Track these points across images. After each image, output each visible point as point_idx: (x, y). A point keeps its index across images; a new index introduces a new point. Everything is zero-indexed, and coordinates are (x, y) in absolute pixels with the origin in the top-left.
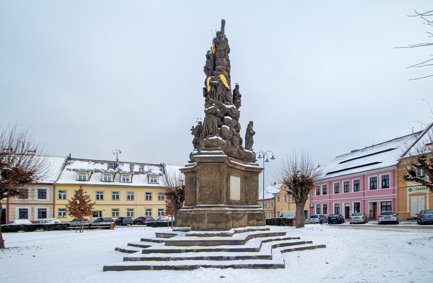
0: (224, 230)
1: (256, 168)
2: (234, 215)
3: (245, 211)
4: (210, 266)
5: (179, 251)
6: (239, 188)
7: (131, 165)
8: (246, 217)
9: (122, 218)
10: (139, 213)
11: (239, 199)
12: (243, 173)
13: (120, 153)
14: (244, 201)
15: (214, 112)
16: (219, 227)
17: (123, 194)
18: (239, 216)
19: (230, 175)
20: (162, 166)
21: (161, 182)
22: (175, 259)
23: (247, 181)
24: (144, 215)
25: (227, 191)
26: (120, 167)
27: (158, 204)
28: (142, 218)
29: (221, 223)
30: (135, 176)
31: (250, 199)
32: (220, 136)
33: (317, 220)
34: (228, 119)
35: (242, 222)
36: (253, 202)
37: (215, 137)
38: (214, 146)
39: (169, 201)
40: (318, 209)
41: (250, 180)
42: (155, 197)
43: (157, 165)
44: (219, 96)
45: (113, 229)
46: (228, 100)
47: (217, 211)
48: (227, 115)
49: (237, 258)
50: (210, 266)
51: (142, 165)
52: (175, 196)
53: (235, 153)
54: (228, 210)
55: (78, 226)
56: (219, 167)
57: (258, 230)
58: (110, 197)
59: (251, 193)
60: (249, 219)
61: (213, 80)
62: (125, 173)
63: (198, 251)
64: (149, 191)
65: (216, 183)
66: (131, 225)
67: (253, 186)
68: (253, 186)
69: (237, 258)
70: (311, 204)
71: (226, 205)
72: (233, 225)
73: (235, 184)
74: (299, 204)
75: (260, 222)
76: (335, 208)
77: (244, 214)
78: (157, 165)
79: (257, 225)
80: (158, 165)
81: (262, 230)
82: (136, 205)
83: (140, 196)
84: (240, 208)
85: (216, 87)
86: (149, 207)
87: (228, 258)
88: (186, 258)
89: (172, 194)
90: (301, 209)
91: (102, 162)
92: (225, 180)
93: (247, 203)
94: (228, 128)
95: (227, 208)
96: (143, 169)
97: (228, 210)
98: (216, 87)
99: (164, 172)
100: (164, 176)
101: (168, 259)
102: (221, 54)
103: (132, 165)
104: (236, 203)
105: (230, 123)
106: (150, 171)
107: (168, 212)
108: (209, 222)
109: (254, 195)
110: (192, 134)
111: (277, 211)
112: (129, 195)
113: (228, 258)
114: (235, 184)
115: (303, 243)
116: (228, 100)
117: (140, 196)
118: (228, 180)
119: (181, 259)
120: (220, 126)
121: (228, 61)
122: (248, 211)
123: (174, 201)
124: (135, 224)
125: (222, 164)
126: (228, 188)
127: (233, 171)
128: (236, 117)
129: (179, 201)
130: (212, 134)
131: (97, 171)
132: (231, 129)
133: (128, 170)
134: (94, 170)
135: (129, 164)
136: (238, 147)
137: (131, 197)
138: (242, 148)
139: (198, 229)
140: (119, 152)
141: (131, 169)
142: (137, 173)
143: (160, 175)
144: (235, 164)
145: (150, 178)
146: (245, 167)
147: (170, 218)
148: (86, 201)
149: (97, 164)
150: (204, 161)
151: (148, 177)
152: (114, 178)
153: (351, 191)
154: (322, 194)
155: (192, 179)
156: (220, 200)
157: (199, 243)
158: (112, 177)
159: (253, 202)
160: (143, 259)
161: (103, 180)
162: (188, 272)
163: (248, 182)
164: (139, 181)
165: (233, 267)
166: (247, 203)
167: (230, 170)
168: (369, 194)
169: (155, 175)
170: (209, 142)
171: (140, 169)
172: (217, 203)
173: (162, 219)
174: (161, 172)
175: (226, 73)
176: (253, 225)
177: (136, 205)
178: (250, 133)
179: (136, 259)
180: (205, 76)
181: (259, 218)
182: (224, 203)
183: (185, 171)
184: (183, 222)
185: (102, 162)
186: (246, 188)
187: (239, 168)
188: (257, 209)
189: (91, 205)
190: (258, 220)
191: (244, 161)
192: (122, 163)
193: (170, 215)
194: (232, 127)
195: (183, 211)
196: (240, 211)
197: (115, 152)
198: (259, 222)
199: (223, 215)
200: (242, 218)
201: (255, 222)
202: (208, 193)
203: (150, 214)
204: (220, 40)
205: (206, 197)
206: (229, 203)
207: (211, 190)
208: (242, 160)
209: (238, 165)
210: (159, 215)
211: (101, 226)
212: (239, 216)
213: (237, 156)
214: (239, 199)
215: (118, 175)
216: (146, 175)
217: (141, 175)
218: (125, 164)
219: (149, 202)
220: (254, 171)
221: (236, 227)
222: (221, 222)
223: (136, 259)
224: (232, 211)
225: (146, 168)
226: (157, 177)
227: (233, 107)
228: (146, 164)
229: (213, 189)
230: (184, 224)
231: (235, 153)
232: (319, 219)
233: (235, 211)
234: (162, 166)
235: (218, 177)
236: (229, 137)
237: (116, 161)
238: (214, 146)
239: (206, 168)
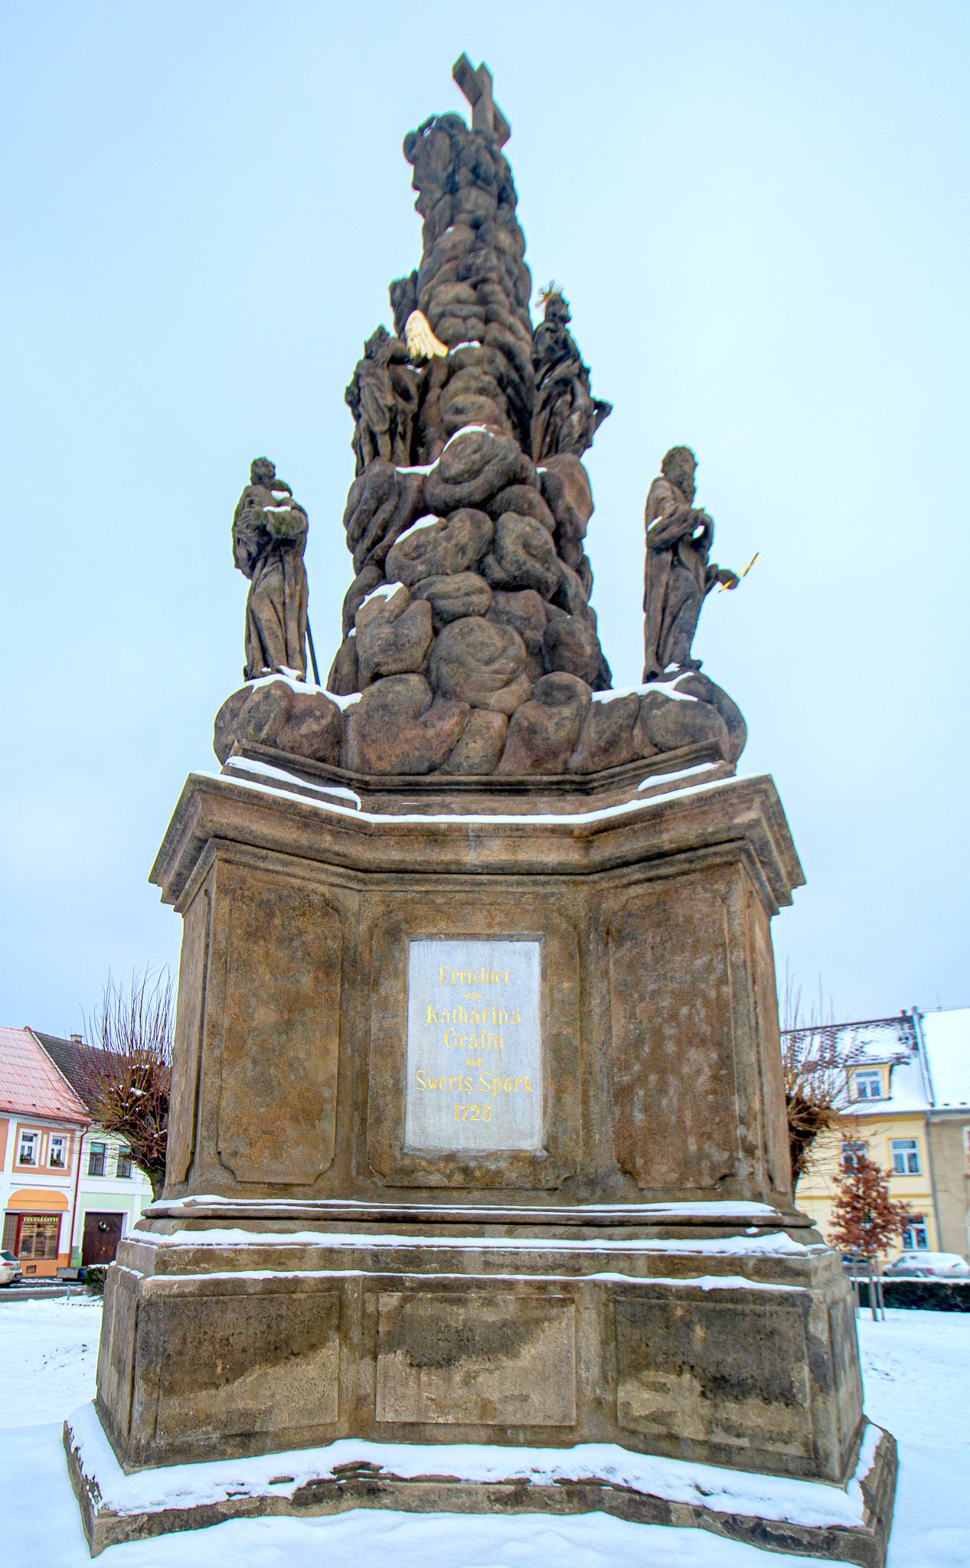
2: (390, 1301)
3: (573, 1263)
8: (575, 1337)
11: (532, 1142)
12: (575, 898)
14: (605, 1158)
18: (459, 1316)
23: (626, 951)
31: (657, 1129)
35: (494, 1382)
36: (687, 1165)
41: (651, 937)
43: (889, 1022)
51: (832, 1031)
59: (662, 1066)
60: (627, 1359)
75: (752, 1414)
77: (552, 1298)
78: (889, 1022)
79: (718, 1455)
80: (894, 1020)
96: (833, 1047)
100: (914, 1062)
104: (470, 1175)
109: (703, 1082)
121: (516, 232)
122: (607, 1261)
143: (899, 1060)
159: (687, 1165)
171: (822, 1049)
173: (910, 1264)
174: (903, 1049)
176: (660, 1441)
178: (681, 549)
181: (736, 1361)
186: (617, 1029)
187: (495, 853)
188: (710, 1247)
190: (718, 1385)
196: (488, 1261)
198: (731, 1410)
200: (504, 1341)
201: (684, 1402)
209: (462, 834)
212: (459, 1316)
220: (666, 839)
224: (376, 1257)
225: (846, 1043)
228: (844, 1026)
233: (412, 1259)
236: (394, 645)
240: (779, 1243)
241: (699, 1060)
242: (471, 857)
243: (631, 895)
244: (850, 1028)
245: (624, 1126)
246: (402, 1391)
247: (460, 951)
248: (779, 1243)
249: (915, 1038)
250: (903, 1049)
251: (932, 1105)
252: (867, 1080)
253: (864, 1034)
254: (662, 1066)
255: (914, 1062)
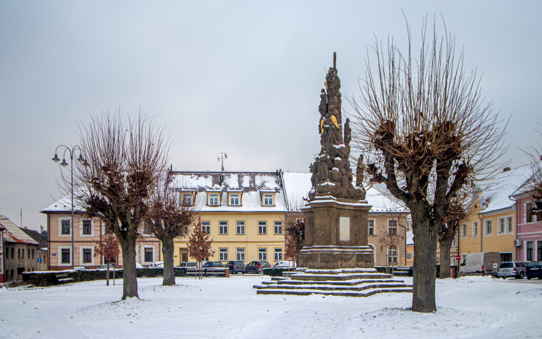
0: (332, 269)
1: (364, 206)
3: (354, 252)
4: (318, 293)
5: (300, 283)
6: (349, 228)
7: (239, 177)
8: (354, 259)
9: (232, 263)
10: (251, 256)
11: (349, 240)
12: (352, 213)
13: (226, 156)
14: (354, 242)
15: (325, 159)
16: (329, 266)
17: (232, 226)
19: (338, 216)
20: (278, 174)
21: (279, 207)
22: (298, 288)
23: (357, 220)
24: (257, 259)
25: (337, 233)
26: (227, 180)
27: (277, 241)
28: (256, 263)
29: (329, 262)
30: (245, 194)
32: (332, 181)
33: (511, 271)
34: (337, 160)
35: (350, 263)
36: (362, 243)
37: (326, 183)
38: (325, 192)
39: (290, 237)
40: (530, 250)
42: (270, 227)
43: (272, 174)
44: (330, 139)
45: (228, 277)
46: (338, 140)
47: (327, 251)
48: (337, 156)
49: (337, 289)
50: (318, 293)
51: (253, 175)
52: (296, 231)
53: (344, 192)
54: (336, 250)
55: (198, 271)
56: (328, 211)
57: (366, 272)
58: (218, 230)
60: (358, 260)
61: (326, 124)
62: (234, 193)
63: (312, 283)
64: (262, 219)
65: (327, 226)
66: (243, 273)
67: (363, 226)
68: (363, 226)
69: (337, 289)
70: (518, 241)
71: (335, 246)
72: (341, 265)
73: (345, 225)
74: (443, 243)
75: (369, 264)
76: (528, 249)
78: (272, 174)
80: (273, 173)
81: (370, 272)
82: (247, 242)
83: (252, 226)
84: (349, 248)
85: (327, 131)
86: (263, 246)
87: (331, 289)
88: (305, 287)
89: (294, 229)
90: (446, 250)
91: (205, 174)
92: (334, 222)
93: (357, 243)
94: (338, 169)
95: (335, 249)
96: (254, 182)
97: (336, 250)
98: (327, 131)
99: (281, 186)
101: (293, 288)
102: (332, 93)
103: (240, 175)
104: (345, 243)
105: (339, 164)
106: (263, 185)
107: (289, 255)
108: (321, 261)
110: (311, 171)
111: (461, 254)
112: (239, 226)
113: (331, 289)
114: (345, 225)
115: (405, 286)
116: (338, 140)
117: (252, 226)
118: (337, 221)
119: (301, 288)
120: (331, 169)
122: (357, 252)
123: (296, 238)
124: (247, 273)
125: (331, 208)
126: (338, 230)
127: (343, 211)
128: (346, 157)
129: (301, 238)
130: (324, 180)
131: (201, 189)
132: (340, 170)
133: (236, 185)
134: (198, 188)
135: (236, 175)
136: (347, 186)
137: (240, 230)
138: (351, 186)
139: (314, 267)
140: (224, 157)
141: (240, 182)
142: (247, 190)
144: (344, 205)
145: (264, 198)
146: (354, 206)
147: (291, 265)
148: (204, 238)
149: (200, 178)
150: (317, 206)
151: (261, 195)
152: (221, 200)
153: (523, 222)
154: (536, 220)
155: (311, 219)
156: (330, 242)
157: (314, 278)
158: (218, 198)
160: (278, 287)
161: (209, 204)
162: (305, 296)
163: (358, 221)
164: (250, 202)
165: (333, 294)
166: (357, 244)
167: (340, 211)
168: (527, 229)
169: (270, 194)
170: (321, 189)
171: (250, 182)
172: (327, 244)
173: (280, 265)
175: (337, 111)
176: (362, 267)
177: (247, 242)
179: (274, 287)
180: (320, 116)
181: (368, 259)
182: (334, 245)
183: (305, 211)
184: (303, 262)
185: (205, 174)
187: (348, 208)
189: (209, 243)
190: (366, 262)
191: (355, 199)
192: (229, 173)
193: (291, 259)
194: (341, 167)
195: (304, 252)
196: (349, 252)
197: (220, 157)
199: (331, 255)
200: (350, 259)
201: (363, 263)
202: (321, 235)
203: (265, 258)
204: (331, 79)
205: (319, 239)
206: (339, 243)
207: (323, 233)
208: (352, 198)
209: (346, 205)
210: (276, 258)
211: (215, 271)
213: (347, 195)
214: (349, 240)
215: (225, 194)
216: (258, 191)
217: (253, 193)
218: (232, 175)
219: (263, 238)
221: (344, 267)
222: (330, 261)
223: (274, 287)
225: (258, 180)
226: (273, 196)
227: (342, 147)
229: (324, 232)
230: (304, 265)
231: (344, 192)
232: (515, 269)
233: (343, 252)
234: (278, 174)
235: (328, 220)
236: (338, 178)
237: (221, 171)
238: (325, 192)
239: (319, 213)
240: (370, 250)
241: (364, 232)
242: (346, 208)
243: (358, 213)
244: (259, 174)
245: (356, 239)
246: (344, 264)
247: (345, 218)
248: (370, 250)
249: (281, 182)
250: (277, 186)
251: (288, 209)
252: (268, 198)
253: (265, 178)
254: (360, 232)
255: (281, 191)
